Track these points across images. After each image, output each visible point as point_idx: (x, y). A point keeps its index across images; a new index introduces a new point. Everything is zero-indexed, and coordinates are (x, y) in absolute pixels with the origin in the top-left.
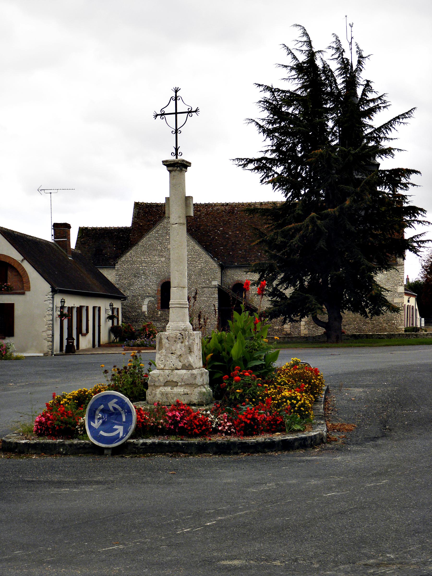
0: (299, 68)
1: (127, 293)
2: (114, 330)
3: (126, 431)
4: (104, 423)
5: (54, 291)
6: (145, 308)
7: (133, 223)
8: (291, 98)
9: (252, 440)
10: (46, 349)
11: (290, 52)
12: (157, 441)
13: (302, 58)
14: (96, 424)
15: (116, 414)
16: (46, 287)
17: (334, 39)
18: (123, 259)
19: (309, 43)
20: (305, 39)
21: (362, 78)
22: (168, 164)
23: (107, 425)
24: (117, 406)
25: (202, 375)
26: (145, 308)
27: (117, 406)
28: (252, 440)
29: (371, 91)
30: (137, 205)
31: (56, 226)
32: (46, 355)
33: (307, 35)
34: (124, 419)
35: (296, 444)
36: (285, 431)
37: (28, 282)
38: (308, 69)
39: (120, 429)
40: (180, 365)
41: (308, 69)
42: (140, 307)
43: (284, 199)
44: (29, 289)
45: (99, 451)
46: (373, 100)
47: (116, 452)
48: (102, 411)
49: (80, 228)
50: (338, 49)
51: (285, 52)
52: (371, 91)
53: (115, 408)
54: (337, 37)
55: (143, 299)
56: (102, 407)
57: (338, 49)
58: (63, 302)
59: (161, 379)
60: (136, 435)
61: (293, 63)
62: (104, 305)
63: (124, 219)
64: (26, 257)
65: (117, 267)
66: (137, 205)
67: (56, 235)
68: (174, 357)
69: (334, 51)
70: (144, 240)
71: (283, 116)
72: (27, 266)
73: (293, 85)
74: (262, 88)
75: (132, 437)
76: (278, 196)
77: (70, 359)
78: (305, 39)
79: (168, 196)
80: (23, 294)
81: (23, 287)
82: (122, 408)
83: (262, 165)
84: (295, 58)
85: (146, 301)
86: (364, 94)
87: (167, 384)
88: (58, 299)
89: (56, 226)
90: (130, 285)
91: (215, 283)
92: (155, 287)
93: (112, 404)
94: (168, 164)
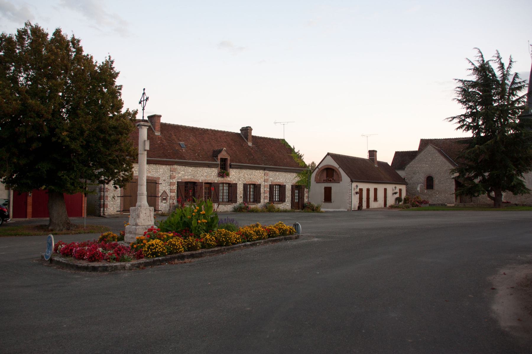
0: (476, 69)
5: (352, 181)
6: (418, 189)
7: (419, 149)
8: (474, 85)
9: (96, 264)
10: (348, 208)
17: (496, 52)
18: (408, 166)
19: (482, 56)
20: (480, 54)
21: (512, 72)
26: (418, 189)
28: (96, 264)
29: (518, 78)
31: (370, 151)
32: (348, 210)
33: (481, 52)
35: (99, 269)
37: (341, 177)
38: (483, 69)
41: (483, 69)
42: (416, 188)
44: (341, 180)
46: (520, 83)
49: (376, 151)
50: (498, 57)
51: (468, 62)
52: (518, 78)
54: (498, 52)
55: (418, 184)
57: (498, 57)
61: (473, 67)
62: (390, 188)
63: (415, 147)
65: (406, 169)
67: (370, 156)
69: (496, 58)
72: (341, 170)
74: (457, 81)
76: (469, 134)
81: (338, 180)
83: (461, 119)
84: (473, 64)
85: (419, 186)
86: (514, 79)
88: (354, 184)
89: (370, 151)
90: (412, 178)
92: (423, 179)
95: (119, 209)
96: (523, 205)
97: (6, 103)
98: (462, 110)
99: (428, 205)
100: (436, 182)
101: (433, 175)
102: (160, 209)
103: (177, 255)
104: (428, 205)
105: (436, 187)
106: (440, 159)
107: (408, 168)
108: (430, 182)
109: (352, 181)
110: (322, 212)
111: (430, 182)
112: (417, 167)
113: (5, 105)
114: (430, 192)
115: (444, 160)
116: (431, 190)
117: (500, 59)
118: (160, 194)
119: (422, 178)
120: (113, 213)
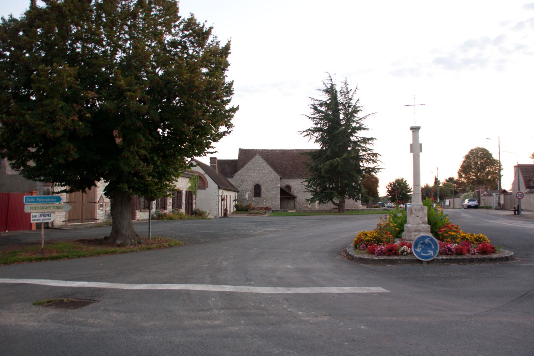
0: (327, 91)
1: (239, 189)
2: (236, 206)
3: (435, 253)
4: (422, 249)
5: (219, 188)
6: (247, 196)
10: (215, 215)
11: (324, 84)
12: (448, 258)
13: (329, 86)
14: (418, 250)
15: (429, 245)
16: (216, 186)
18: (237, 174)
19: (331, 80)
20: (329, 78)
22: (412, 128)
23: (424, 250)
24: (429, 241)
25: (427, 227)
26: (247, 196)
27: (429, 241)
30: (240, 149)
32: (215, 217)
34: (433, 247)
36: (374, 254)
37: (207, 184)
38: (331, 91)
39: (431, 252)
40: (421, 222)
41: (331, 91)
42: (245, 196)
43: (320, 148)
44: (207, 187)
45: (421, 262)
47: (428, 262)
48: (422, 244)
50: (345, 83)
53: (428, 243)
55: (246, 192)
56: (422, 242)
57: (345, 83)
58: (223, 193)
59: (413, 228)
60: (440, 254)
63: (235, 156)
64: (206, 173)
66: (240, 149)
67: (211, 163)
68: (418, 218)
70: (247, 165)
71: (319, 112)
72: (207, 176)
73: (325, 98)
75: (437, 256)
77: (226, 219)
78: (329, 78)
79: (412, 143)
80: (205, 189)
82: (432, 242)
85: (247, 193)
87: (415, 231)
88: (221, 191)
90: (240, 185)
91: (279, 185)
93: (426, 241)
94: (412, 128)
95: (64, 219)
96: (353, 210)
97: (89, 68)
98: (311, 125)
99: (271, 211)
100: (263, 190)
101: (260, 183)
102: (98, 218)
103: (403, 258)
104: (271, 211)
105: (263, 195)
106: (268, 169)
107: (237, 176)
108: (257, 190)
109: (219, 188)
110: (209, 219)
111: (257, 190)
112: (245, 176)
113: (91, 70)
114: (257, 199)
115: (271, 169)
116: (258, 198)
117: (346, 85)
118: (98, 200)
119: (250, 187)
120: (59, 224)
